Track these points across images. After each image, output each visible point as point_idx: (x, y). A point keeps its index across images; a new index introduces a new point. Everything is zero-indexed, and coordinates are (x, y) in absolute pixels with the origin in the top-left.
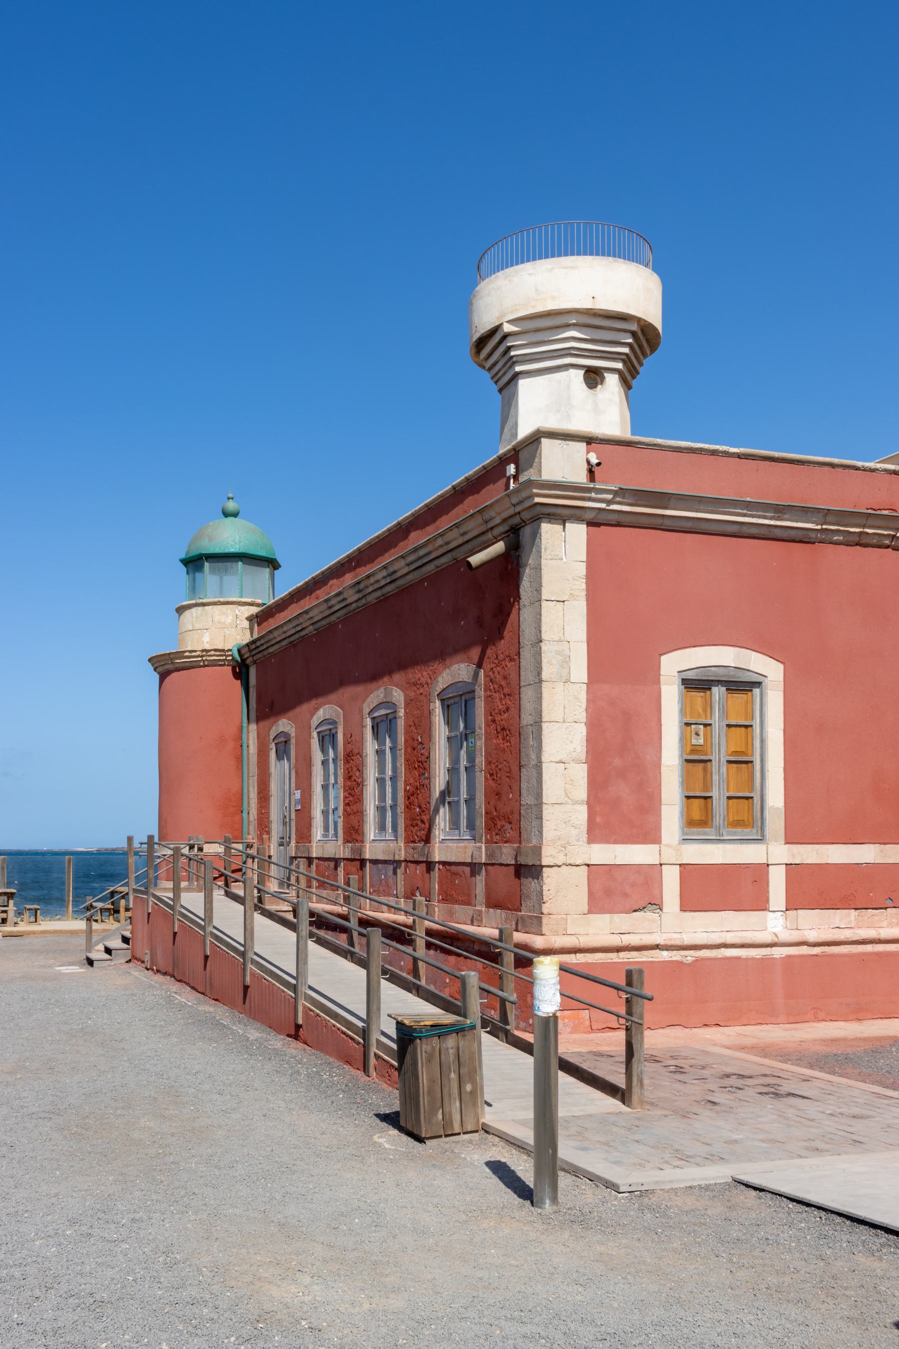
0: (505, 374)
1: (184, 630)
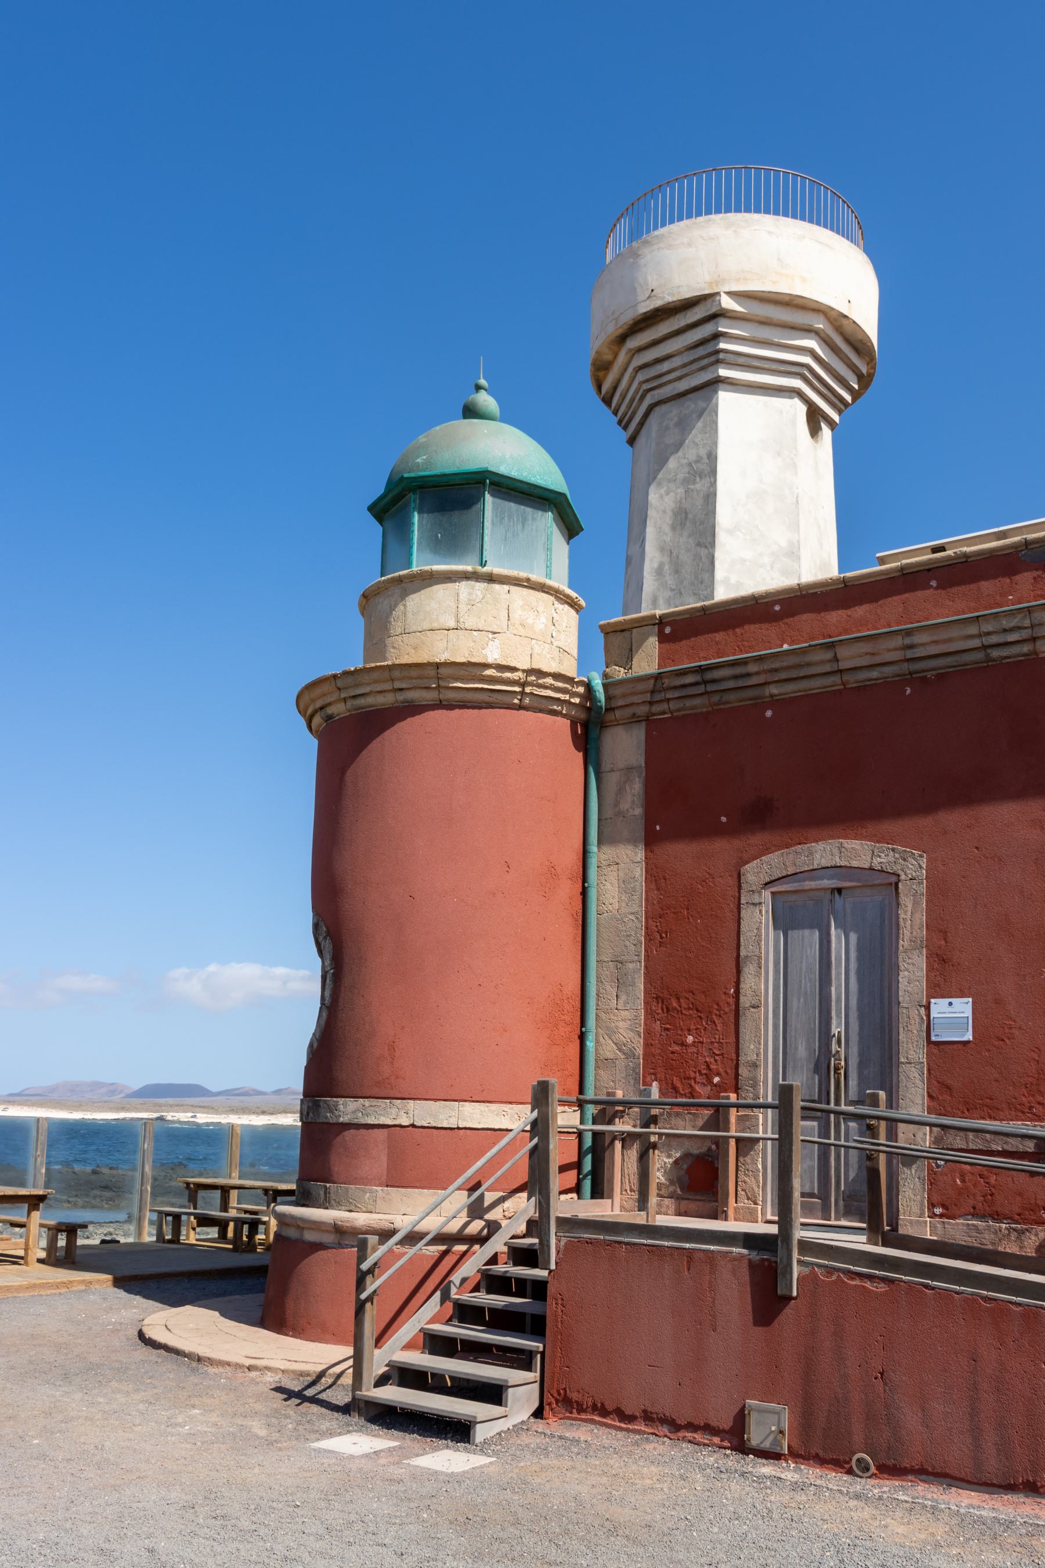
0: (680, 378)
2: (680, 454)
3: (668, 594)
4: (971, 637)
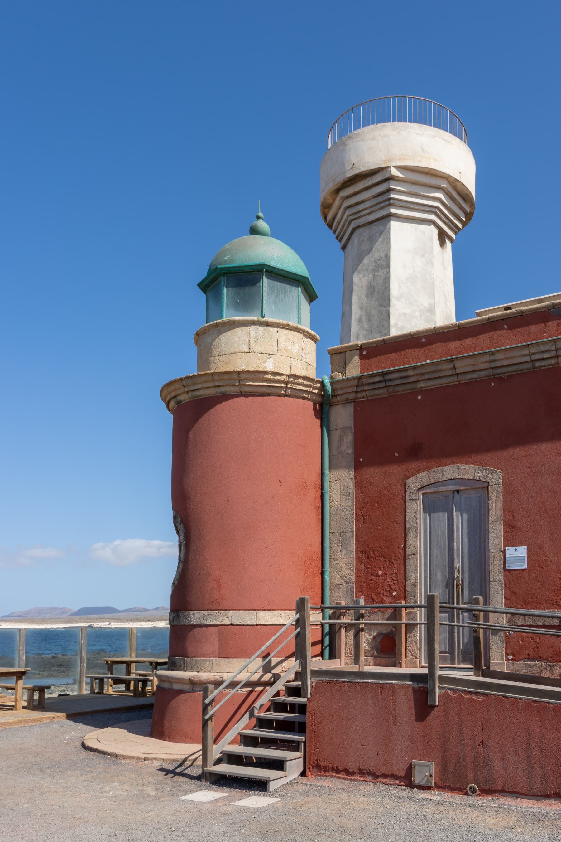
1: (232, 350)
2: (370, 255)
3: (365, 332)
4: (525, 355)
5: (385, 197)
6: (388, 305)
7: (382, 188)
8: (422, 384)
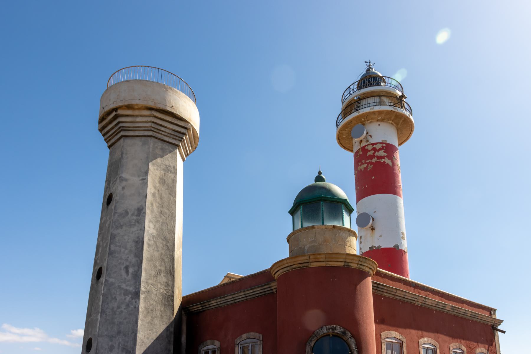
0: (165, 136)
2: (162, 159)
3: (158, 205)
5: (181, 135)
6: (175, 197)
7: (183, 130)
8: (385, 294)
